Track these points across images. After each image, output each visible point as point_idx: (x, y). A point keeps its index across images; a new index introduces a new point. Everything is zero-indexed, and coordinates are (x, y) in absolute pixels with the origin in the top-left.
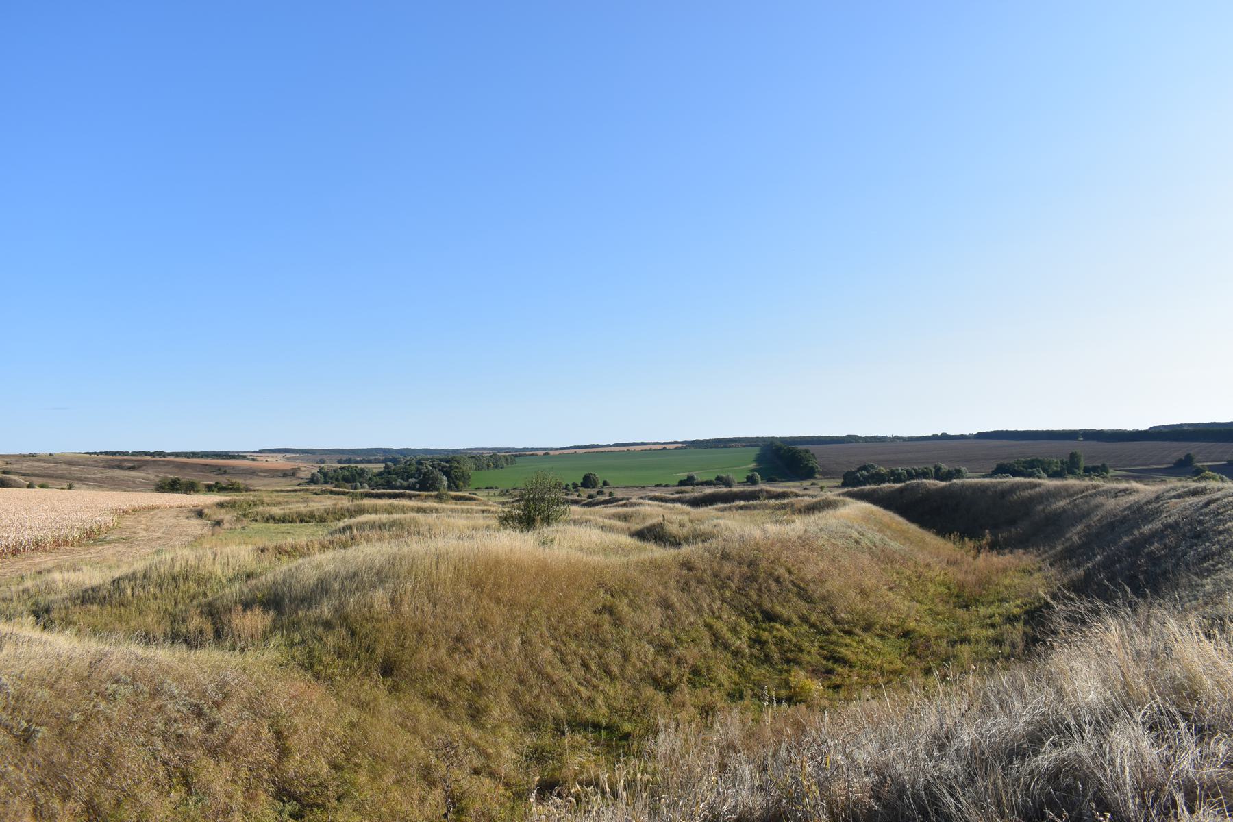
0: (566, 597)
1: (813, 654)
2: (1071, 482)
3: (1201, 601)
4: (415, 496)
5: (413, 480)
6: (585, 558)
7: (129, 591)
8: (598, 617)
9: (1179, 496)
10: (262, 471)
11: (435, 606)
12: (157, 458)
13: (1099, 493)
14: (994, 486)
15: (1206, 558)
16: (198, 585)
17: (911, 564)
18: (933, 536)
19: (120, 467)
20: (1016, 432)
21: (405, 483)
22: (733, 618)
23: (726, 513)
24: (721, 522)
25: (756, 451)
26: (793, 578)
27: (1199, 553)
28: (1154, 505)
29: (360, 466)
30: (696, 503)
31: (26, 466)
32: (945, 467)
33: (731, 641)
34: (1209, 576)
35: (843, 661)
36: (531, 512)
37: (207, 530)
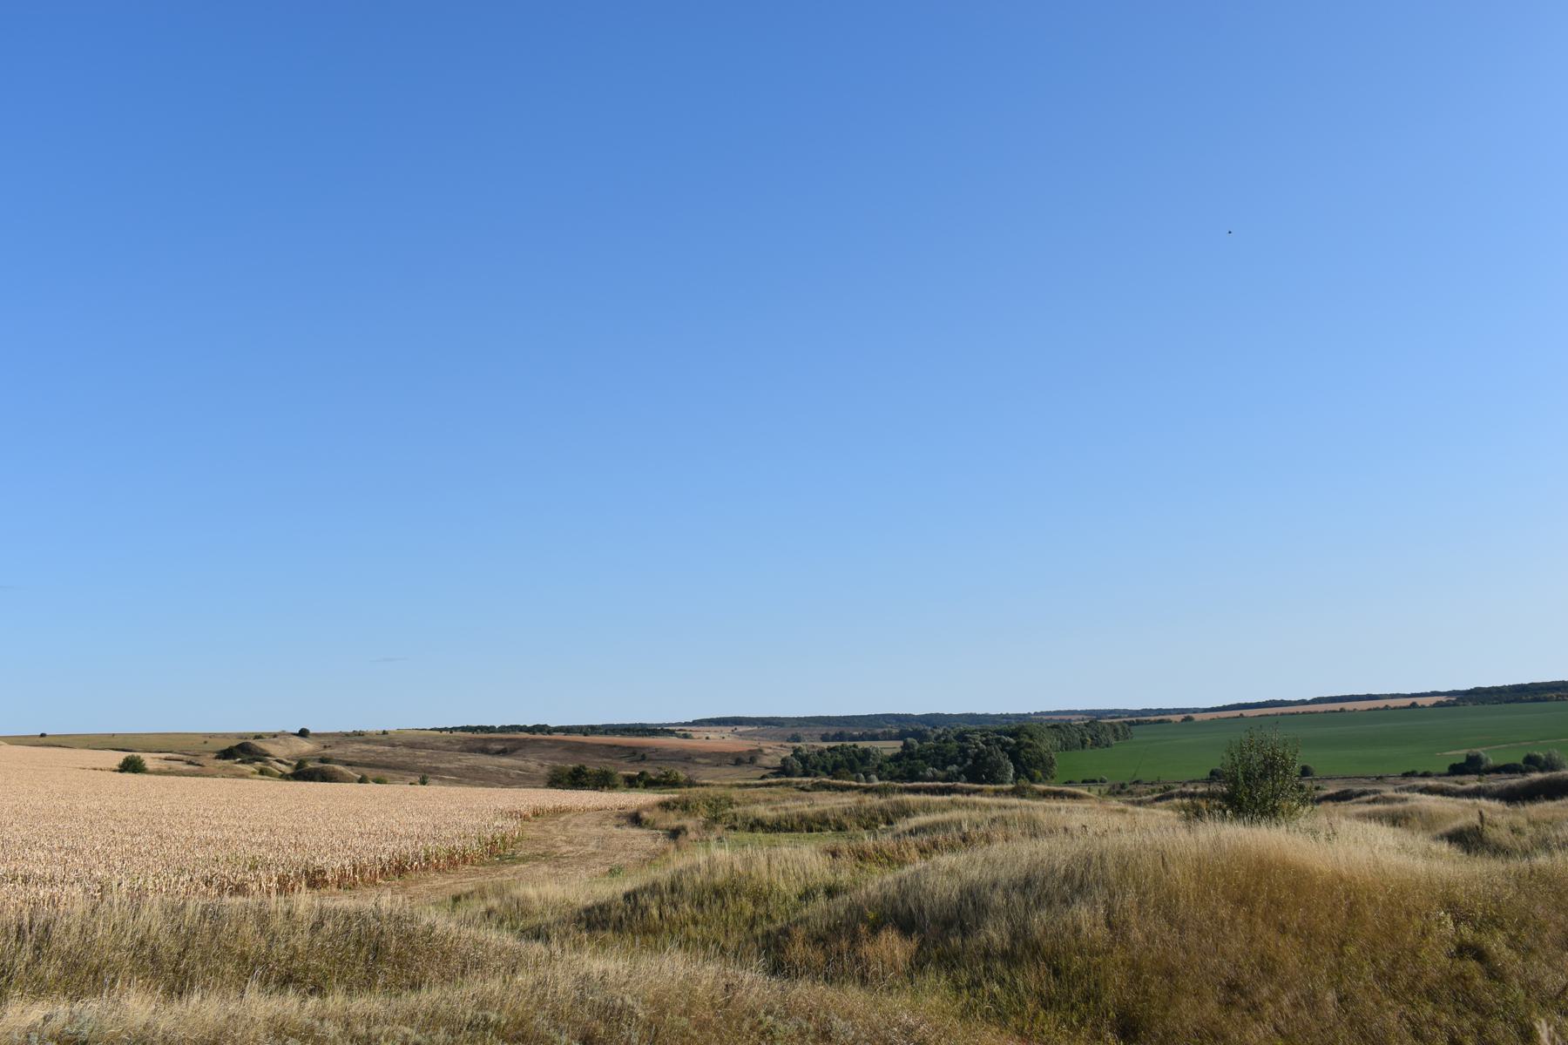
5: (954, 768)
7: (655, 912)
10: (706, 755)
12: (538, 736)
16: (755, 903)
19: (485, 751)
21: (940, 774)
29: (861, 745)
31: (352, 751)
37: (661, 843)
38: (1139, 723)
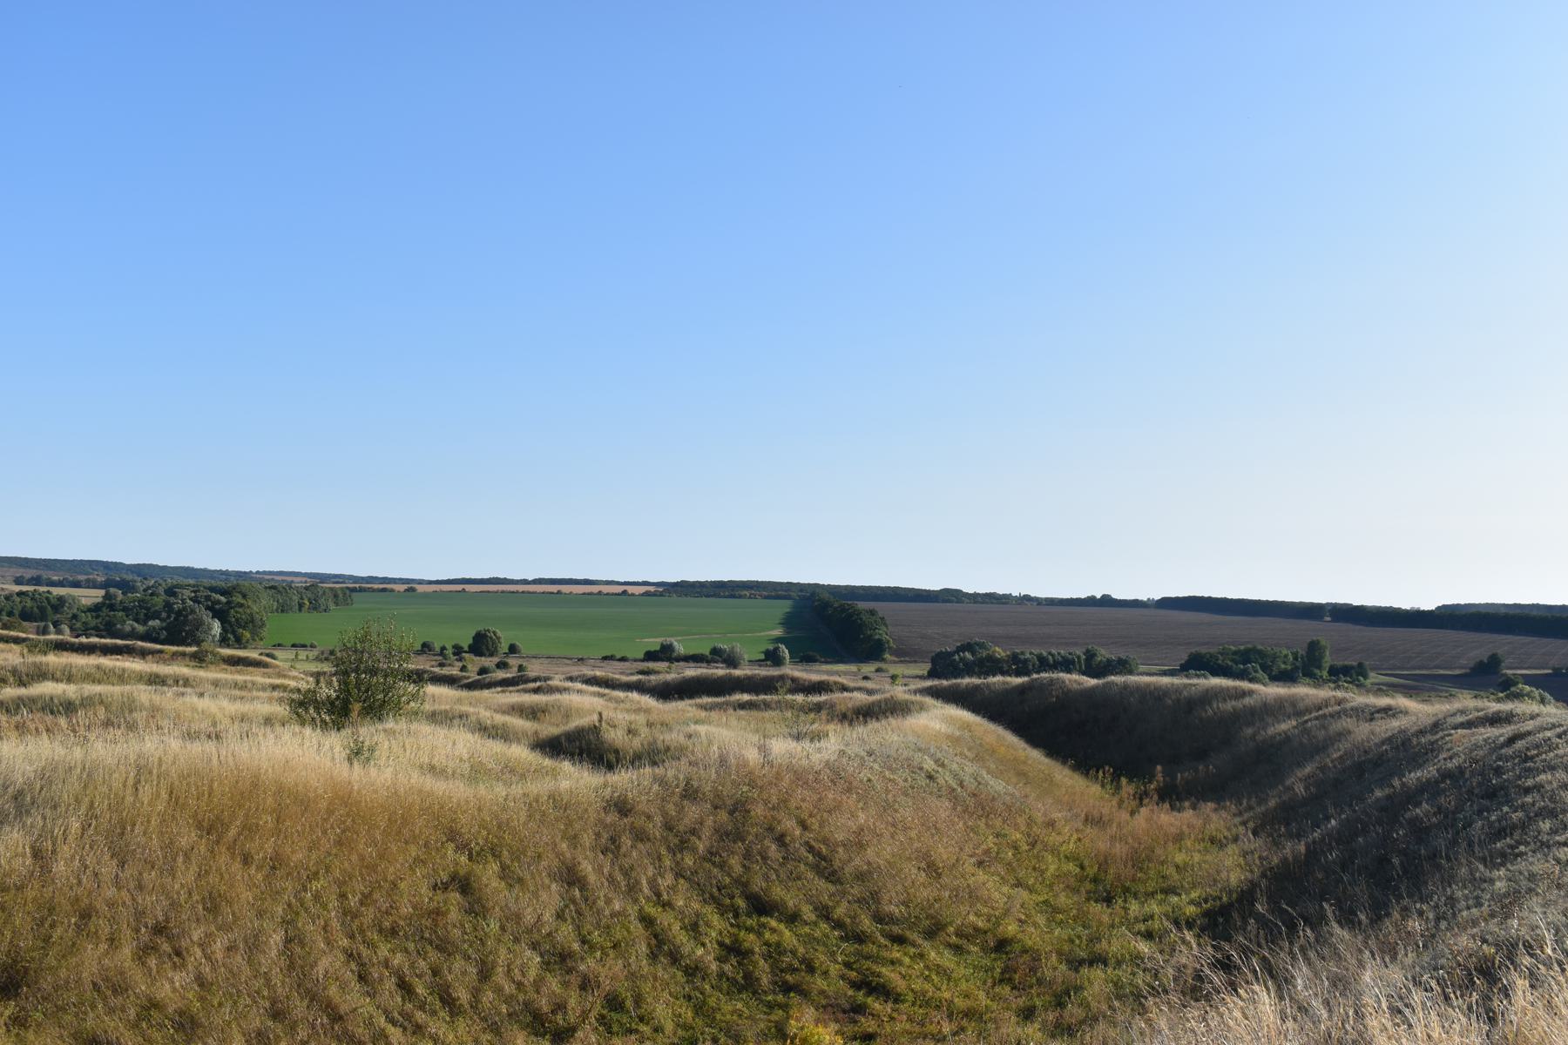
0: (381, 856)
1: (831, 980)
2: (1303, 691)
3: (1485, 908)
4: (153, 652)
5: (155, 623)
6: (439, 787)
8: (440, 896)
9: (1469, 725)
11: (122, 864)
13: (1344, 713)
14: (1178, 690)
15: (1500, 833)
17: (1021, 821)
18: (1067, 771)
20: (1177, 599)
21: (140, 628)
22: (696, 906)
23: (714, 715)
24: (702, 729)
25: (784, 607)
26: (809, 836)
27: (1491, 825)
28: (1429, 737)
29: (57, 591)
30: (666, 692)
32: (1104, 654)
33: (686, 950)
34: (1503, 864)
35: (882, 991)
36: (354, 694)
38: (361, 590)
